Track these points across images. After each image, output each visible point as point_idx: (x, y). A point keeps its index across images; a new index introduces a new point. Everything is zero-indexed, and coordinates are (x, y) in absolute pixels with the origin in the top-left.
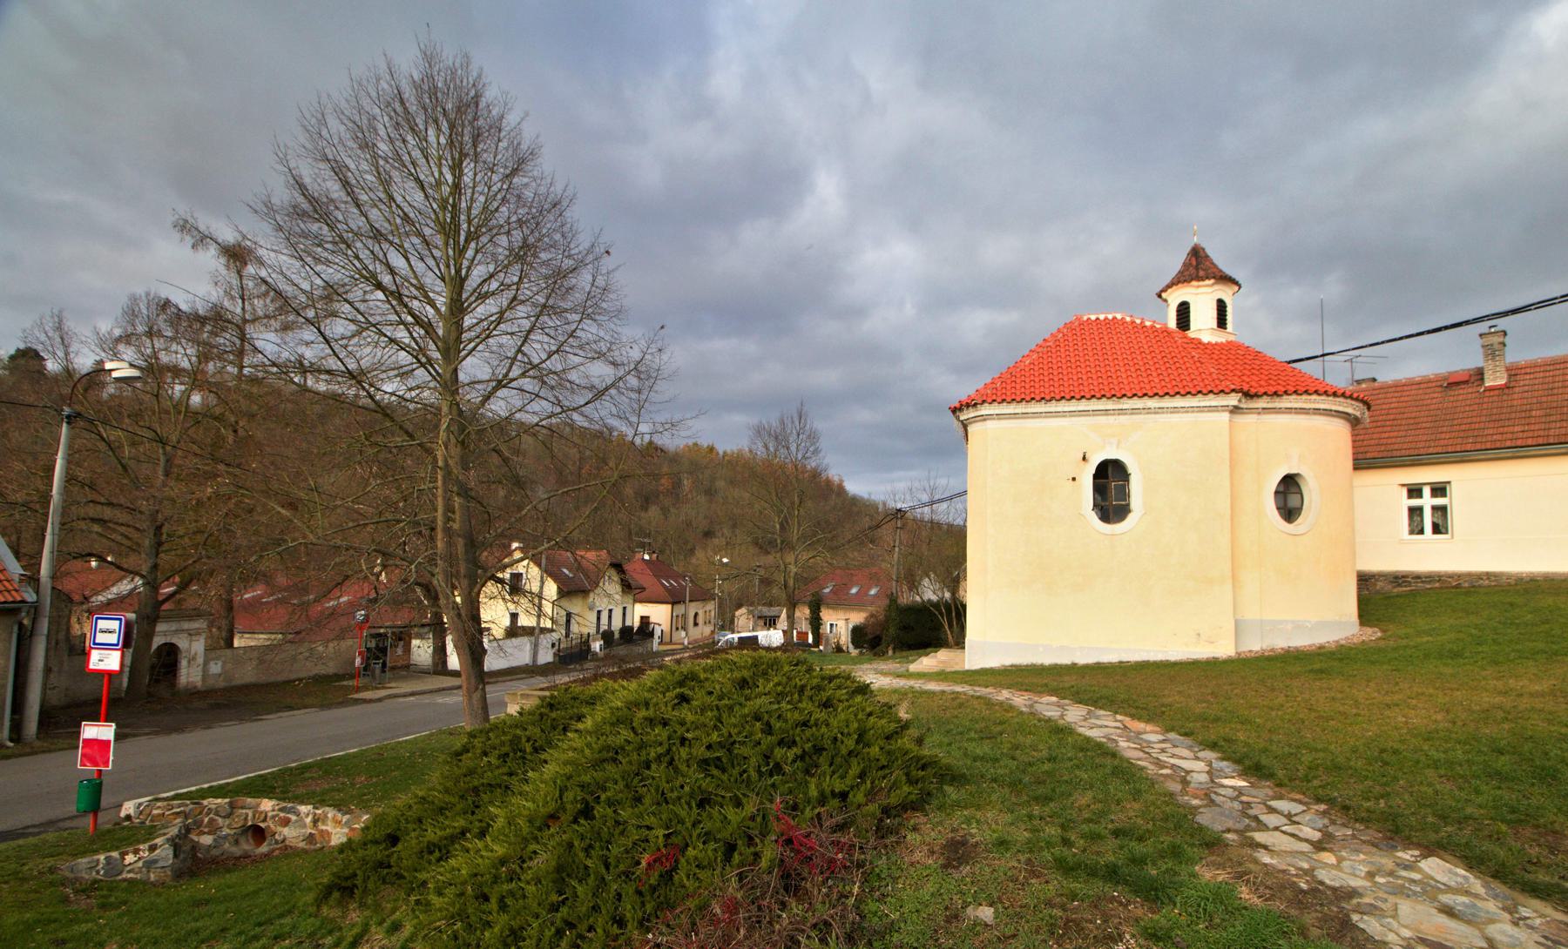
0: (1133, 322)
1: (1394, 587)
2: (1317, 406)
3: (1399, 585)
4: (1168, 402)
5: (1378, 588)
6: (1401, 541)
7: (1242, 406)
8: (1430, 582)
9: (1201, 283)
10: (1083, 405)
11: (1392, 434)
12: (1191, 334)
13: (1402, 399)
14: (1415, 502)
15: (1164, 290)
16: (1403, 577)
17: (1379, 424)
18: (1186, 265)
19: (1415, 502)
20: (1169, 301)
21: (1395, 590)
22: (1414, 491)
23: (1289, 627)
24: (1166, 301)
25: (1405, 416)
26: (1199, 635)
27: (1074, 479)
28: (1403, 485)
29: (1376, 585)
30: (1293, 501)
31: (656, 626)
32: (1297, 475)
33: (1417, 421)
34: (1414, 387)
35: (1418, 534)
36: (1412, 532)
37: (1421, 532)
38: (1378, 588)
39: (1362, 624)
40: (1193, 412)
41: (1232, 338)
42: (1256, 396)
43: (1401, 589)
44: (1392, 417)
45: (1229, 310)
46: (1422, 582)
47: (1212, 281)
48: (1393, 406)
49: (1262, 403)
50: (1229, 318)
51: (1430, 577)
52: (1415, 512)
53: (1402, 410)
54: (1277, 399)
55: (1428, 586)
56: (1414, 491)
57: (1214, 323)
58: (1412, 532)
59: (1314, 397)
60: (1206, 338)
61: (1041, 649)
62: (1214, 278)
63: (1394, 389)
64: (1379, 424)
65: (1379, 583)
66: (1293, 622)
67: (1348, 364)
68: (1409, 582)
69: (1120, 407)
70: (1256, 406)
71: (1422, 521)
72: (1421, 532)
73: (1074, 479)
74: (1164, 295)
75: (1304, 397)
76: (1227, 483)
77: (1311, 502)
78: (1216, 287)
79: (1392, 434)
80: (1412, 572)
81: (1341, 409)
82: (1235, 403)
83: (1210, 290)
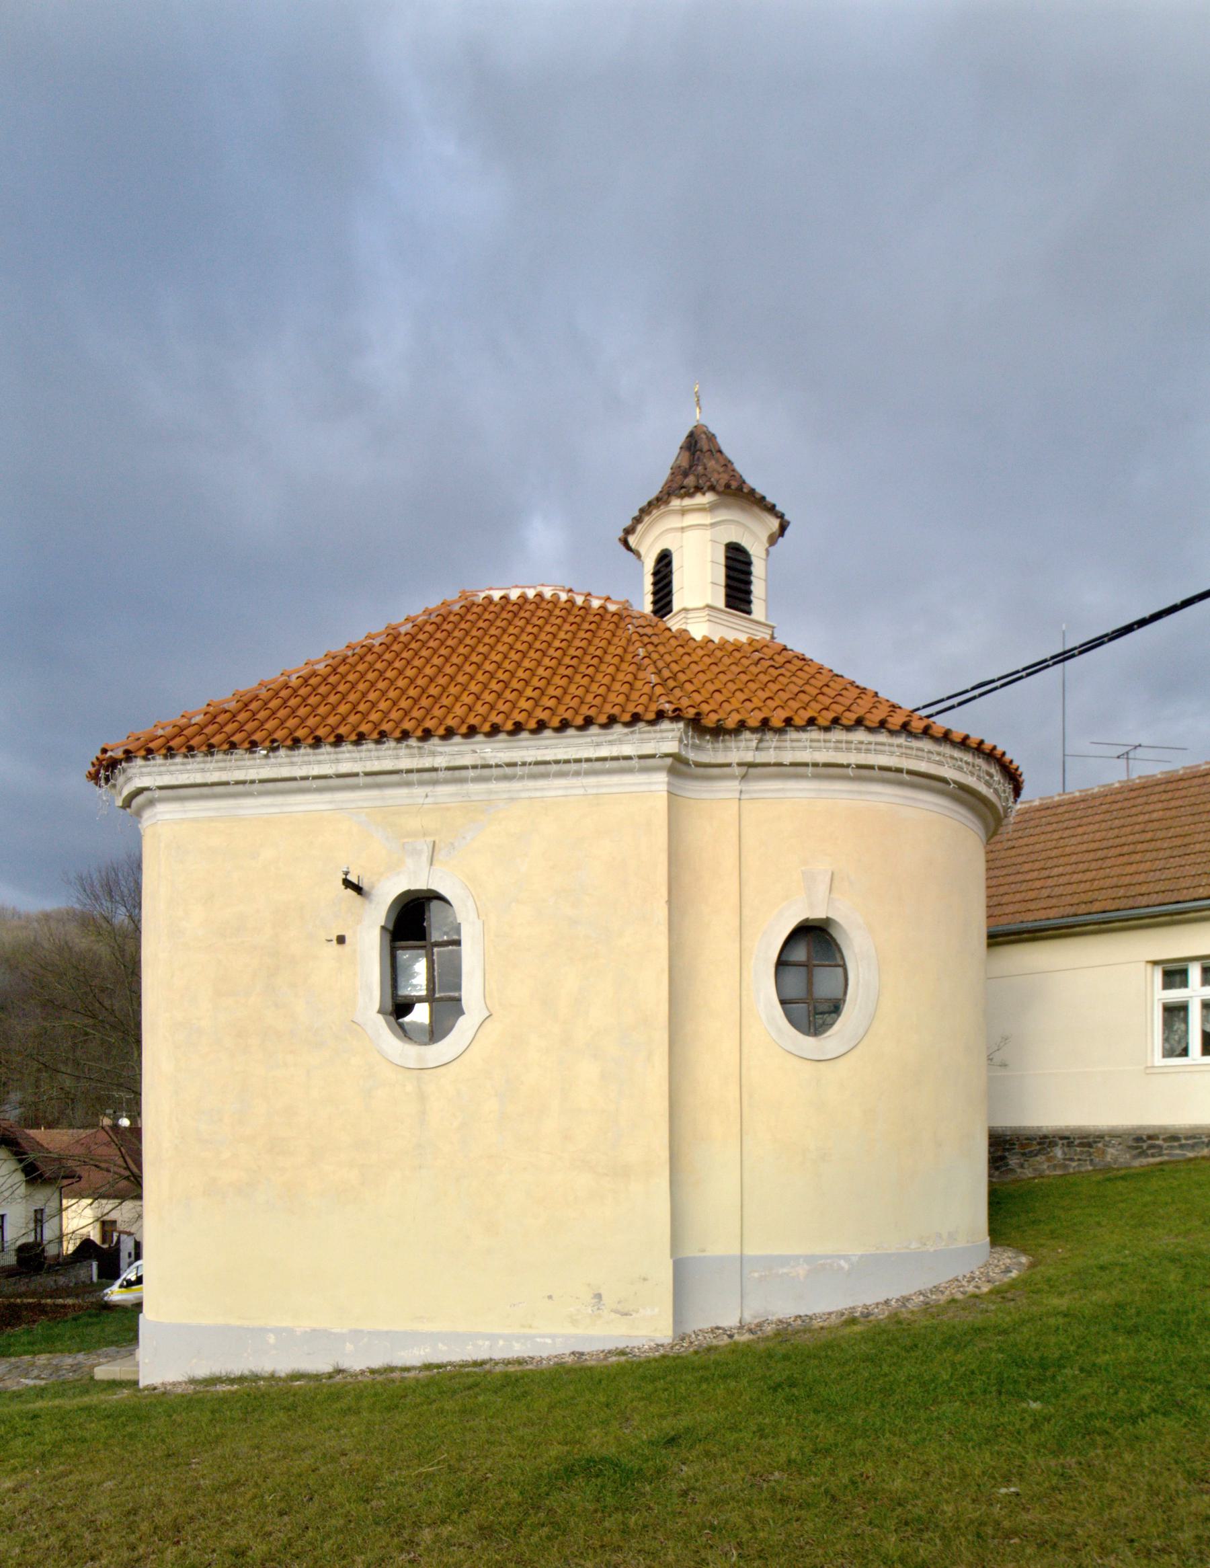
0: (571, 601)
1: (1135, 1157)
2: (863, 759)
3: (1143, 1154)
4: (528, 749)
5: (1109, 1158)
6: (1150, 1070)
7: (692, 756)
8: (1193, 1146)
9: (687, 502)
10: (349, 760)
11: (1142, 867)
12: (674, 623)
13: (1173, 804)
14: (1175, 995)
15: (629, 531)
16: (1150, 1137)
17: (1126, 849)
18: (680, 472)
19: (1175, 995)
20: (642, 551)
21: (1136, 1163)
22: (1174, 975)
23: (802, 1270)
24: (638, 554)
25: (1171, 833)
26: (599, 1296)
27: (341, 940)
28: (1155, 963)
29: (1104, 1153)
30: (825, 981)
31: (123, 1237)
32: (828, 921)
33: (1186, 840)
34: (1196, 781)
35: (1180, 1055)
36: (1169, 1053)
37: (1185, 1052)
38: (1109, 1158)
39: (994, 1242)
40: (577, 774)
41: (762, 635)
42: (718, 731)
43: (1144, 1161)
44: (1149, 836)
45: (758, 569)
46: (1182, 1147)
47: (707, 498)
48: (1155, 816)
49: (741, 750)
50: (758, 589)
51: (1193, 1137)
52: (1175, 1013)
53: (1169, 823)
54: (771, 739)
55: (1190, 1155)
56: (1174, 975)
57: (718, 598)
58: (1169, 1053)
59: (860, 735)
60: (699, 630)
61: (272, 1339)
62: (712, 488)
63: (1162, 788)
64: (1126, 849)
65: (1110, 1150)
66: (809, 1259)
67: (1123, 762)
68: (1160, 1147)
69: (427, 762)
70: (720, 758)
71: (1186, 1032)
72: (1185, 1052)
73: (341, 940)
74: (632, 540)
75: (838, 735)
76: (662, 941)
77: (857, 983)
78: (723, 515)
79: (1142, 867)
80: (1164, 1129)
81: (923, 767)
82: (671, 747)
83: (706, 519)
